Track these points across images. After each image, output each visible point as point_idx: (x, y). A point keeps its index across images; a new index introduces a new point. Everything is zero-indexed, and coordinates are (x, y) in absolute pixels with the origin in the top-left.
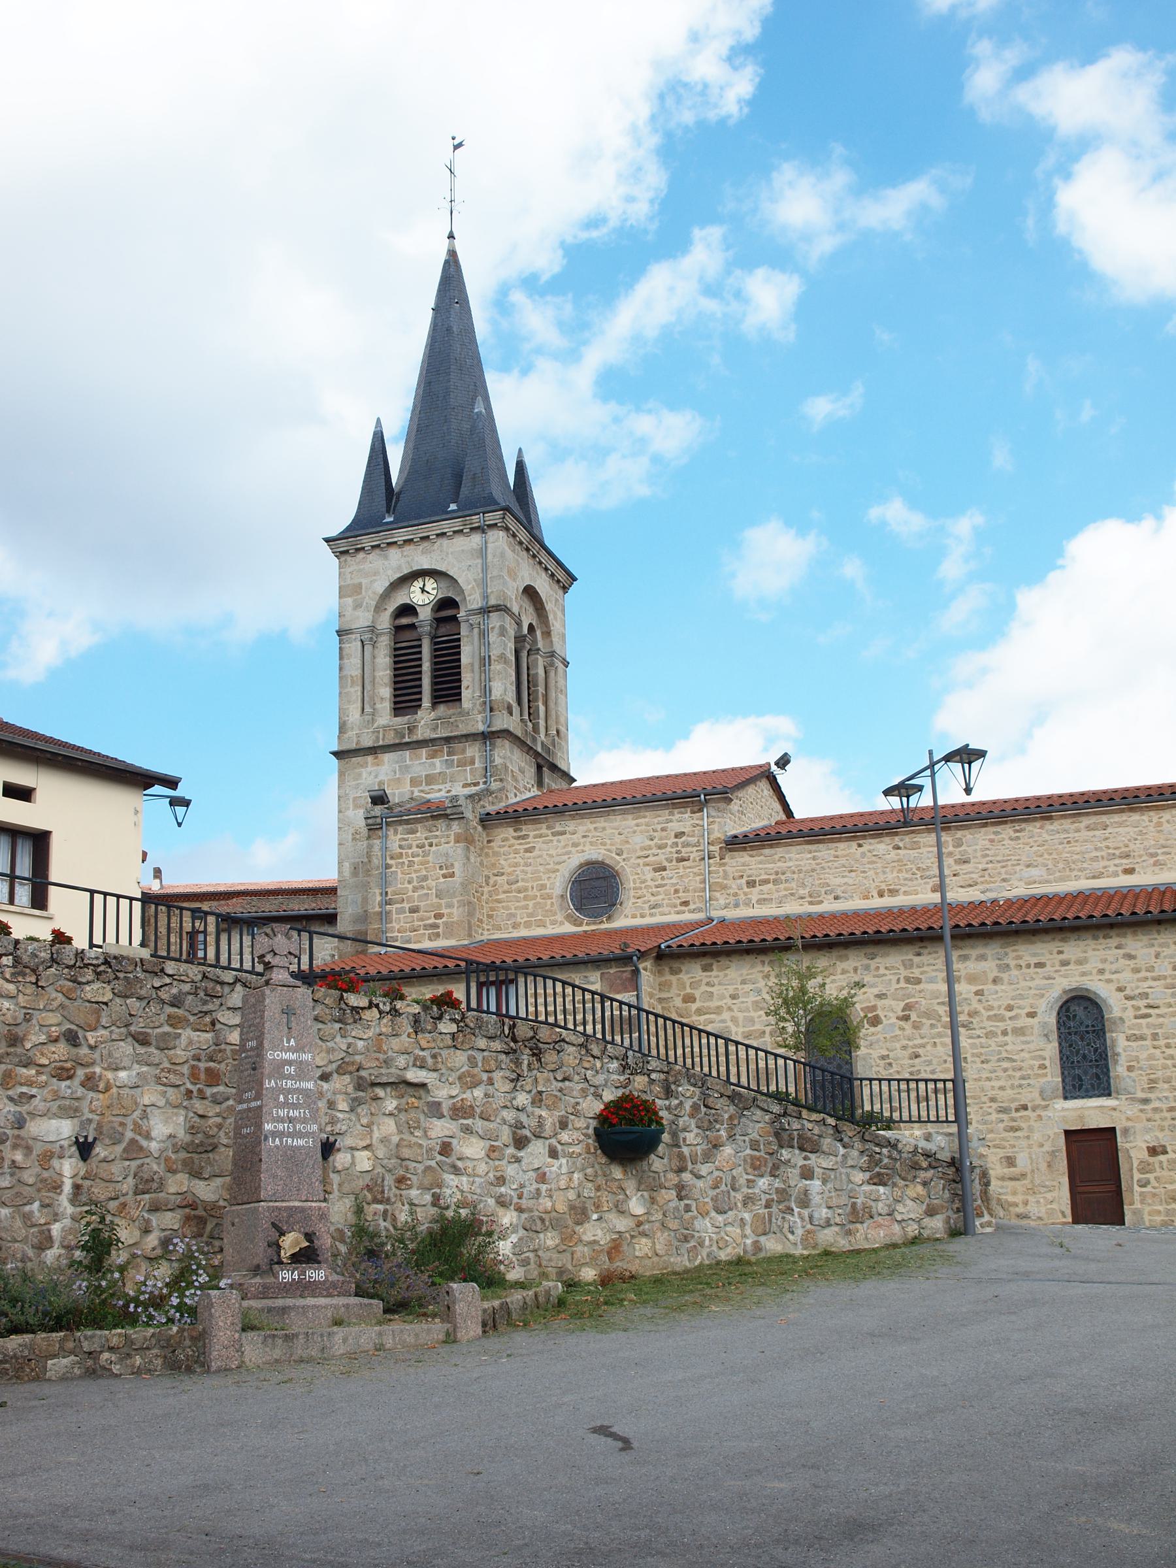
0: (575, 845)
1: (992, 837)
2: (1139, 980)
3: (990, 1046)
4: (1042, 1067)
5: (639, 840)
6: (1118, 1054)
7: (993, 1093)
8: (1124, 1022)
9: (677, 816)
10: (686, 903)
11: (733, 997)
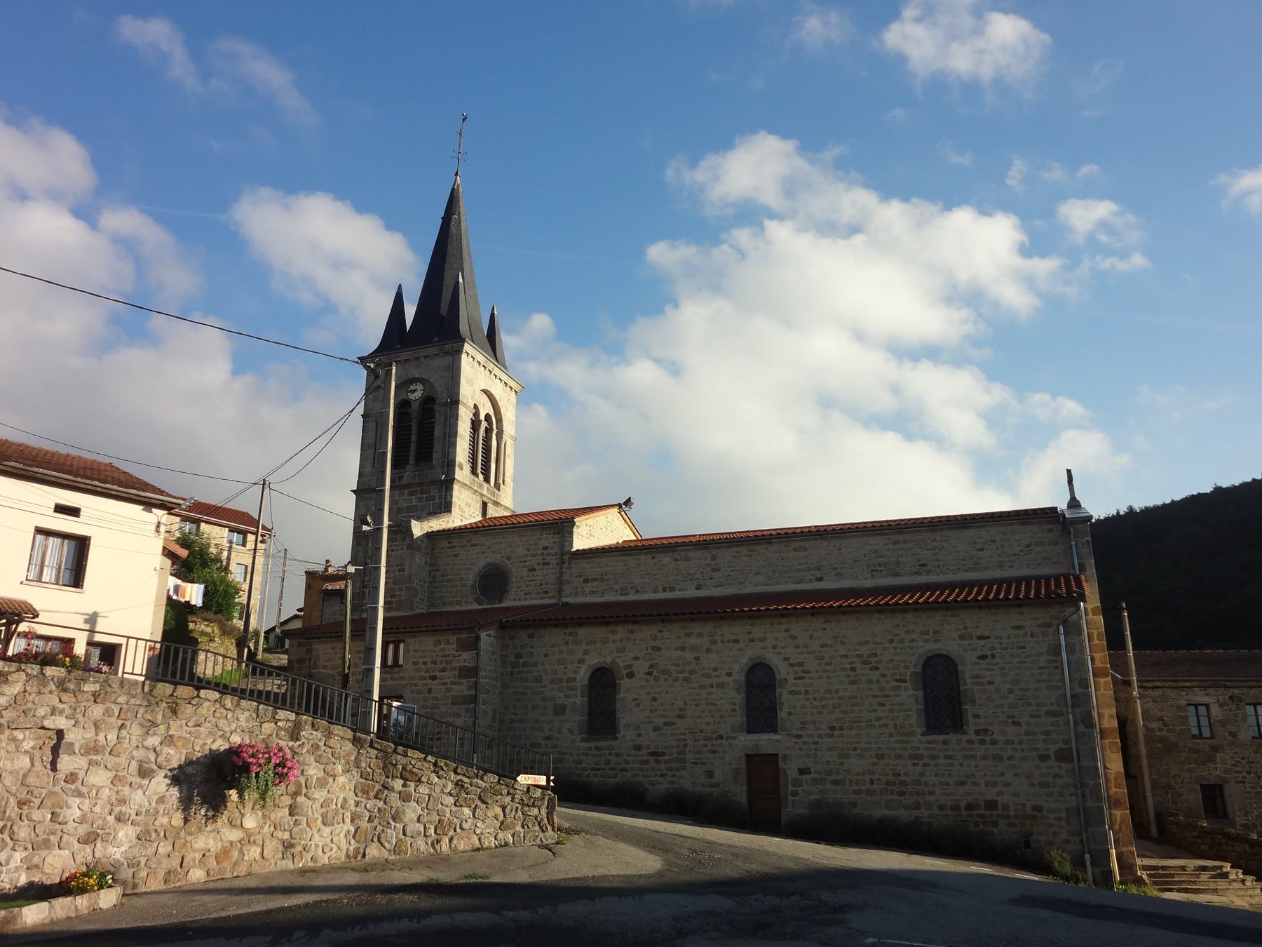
0: (483, 553)
1: (735, 554)
2: (799, 653)
3: (702, 695)
4: (734, 710)
5: (521, 551)
6: (782, 704)
7: (702, 726)
8: (787, 681)
9: (545, 536)
10: (546, 592)
11: (546, 656)
